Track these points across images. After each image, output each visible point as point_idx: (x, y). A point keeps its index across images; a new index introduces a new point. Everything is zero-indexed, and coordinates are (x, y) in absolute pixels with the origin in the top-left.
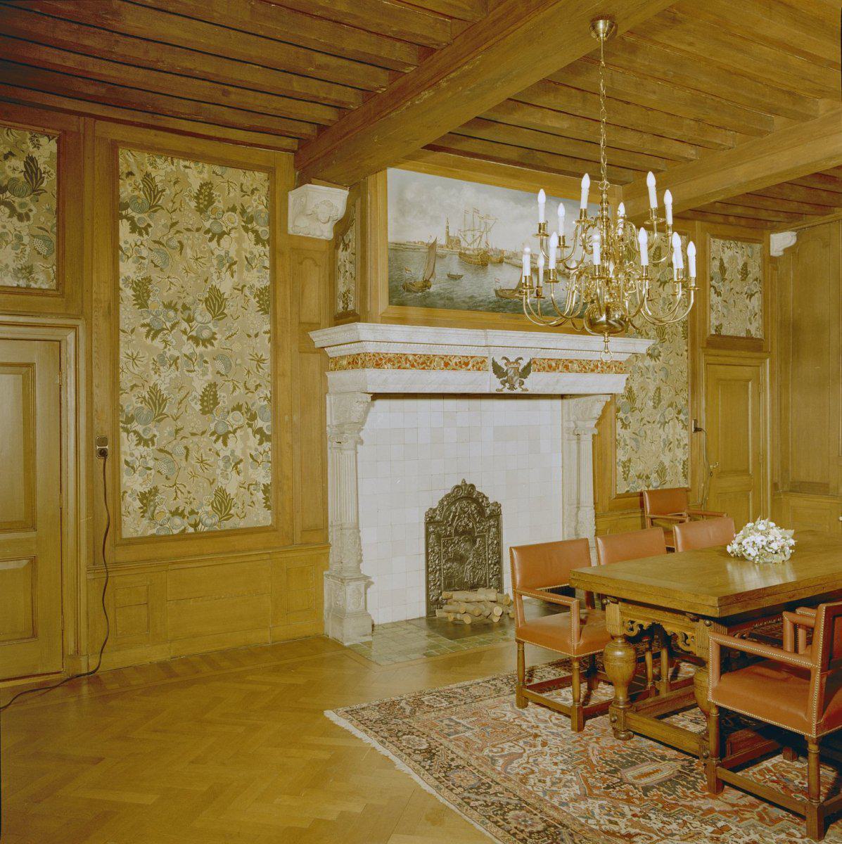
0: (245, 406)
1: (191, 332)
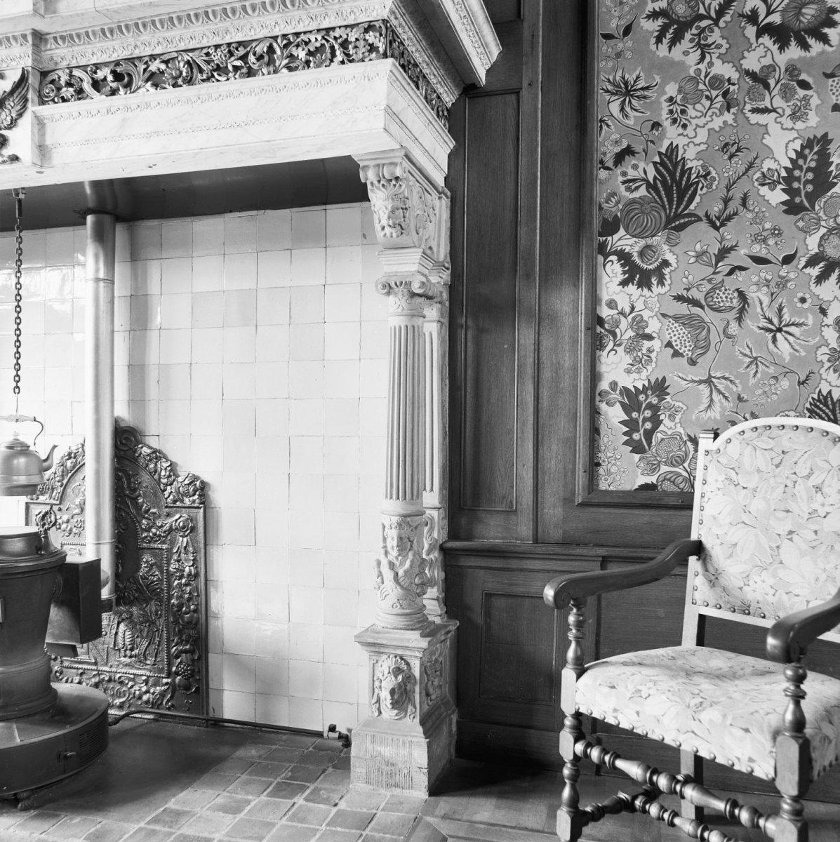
1: (768, 14)
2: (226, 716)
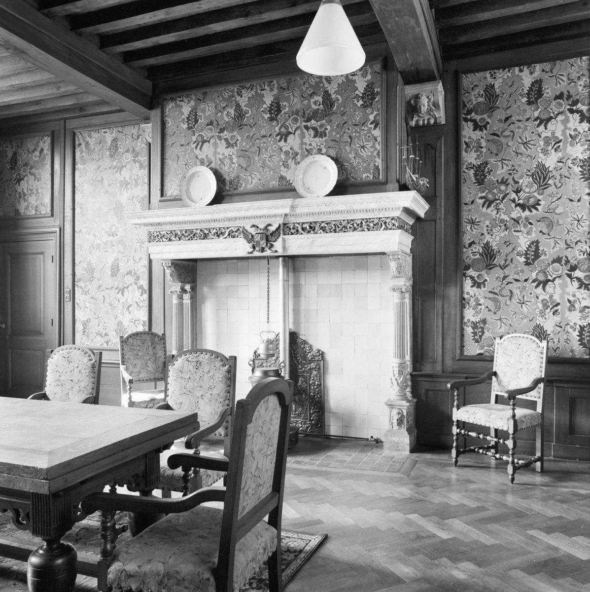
0: (564, 258)
2: (331, 434)
